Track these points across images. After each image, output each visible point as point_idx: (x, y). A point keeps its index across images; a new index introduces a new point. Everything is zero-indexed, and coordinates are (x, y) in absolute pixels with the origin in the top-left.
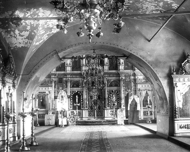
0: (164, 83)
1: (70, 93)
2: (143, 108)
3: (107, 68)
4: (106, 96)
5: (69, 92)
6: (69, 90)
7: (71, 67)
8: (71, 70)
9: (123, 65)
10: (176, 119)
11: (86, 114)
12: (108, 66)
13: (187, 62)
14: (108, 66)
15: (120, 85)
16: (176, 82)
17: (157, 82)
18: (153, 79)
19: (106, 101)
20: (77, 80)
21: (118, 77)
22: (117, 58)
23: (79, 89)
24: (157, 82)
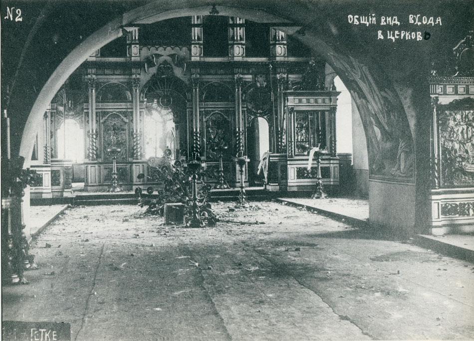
0: (405, 98)
1: (97, 116)
2: (308, 160)
3: (283, 49)
4: (196, 125)
5: (94, 113)
6: (94, 107)
7: (244, 47)
8: (99, 55)
9: (242, 42)
10: (433, 190)
11: (464, 200)
12: (201, 44)
13: (464, 43)
14: (244, 47)
15: (233, 96)
16: (436, 94)
17: (385, 95)
18: (370, 84)
19: (196, 139)
20: (115, 81)
21: (231, 76)
22: (266, 27)
23: (121, 105)
24: (385, 95)
